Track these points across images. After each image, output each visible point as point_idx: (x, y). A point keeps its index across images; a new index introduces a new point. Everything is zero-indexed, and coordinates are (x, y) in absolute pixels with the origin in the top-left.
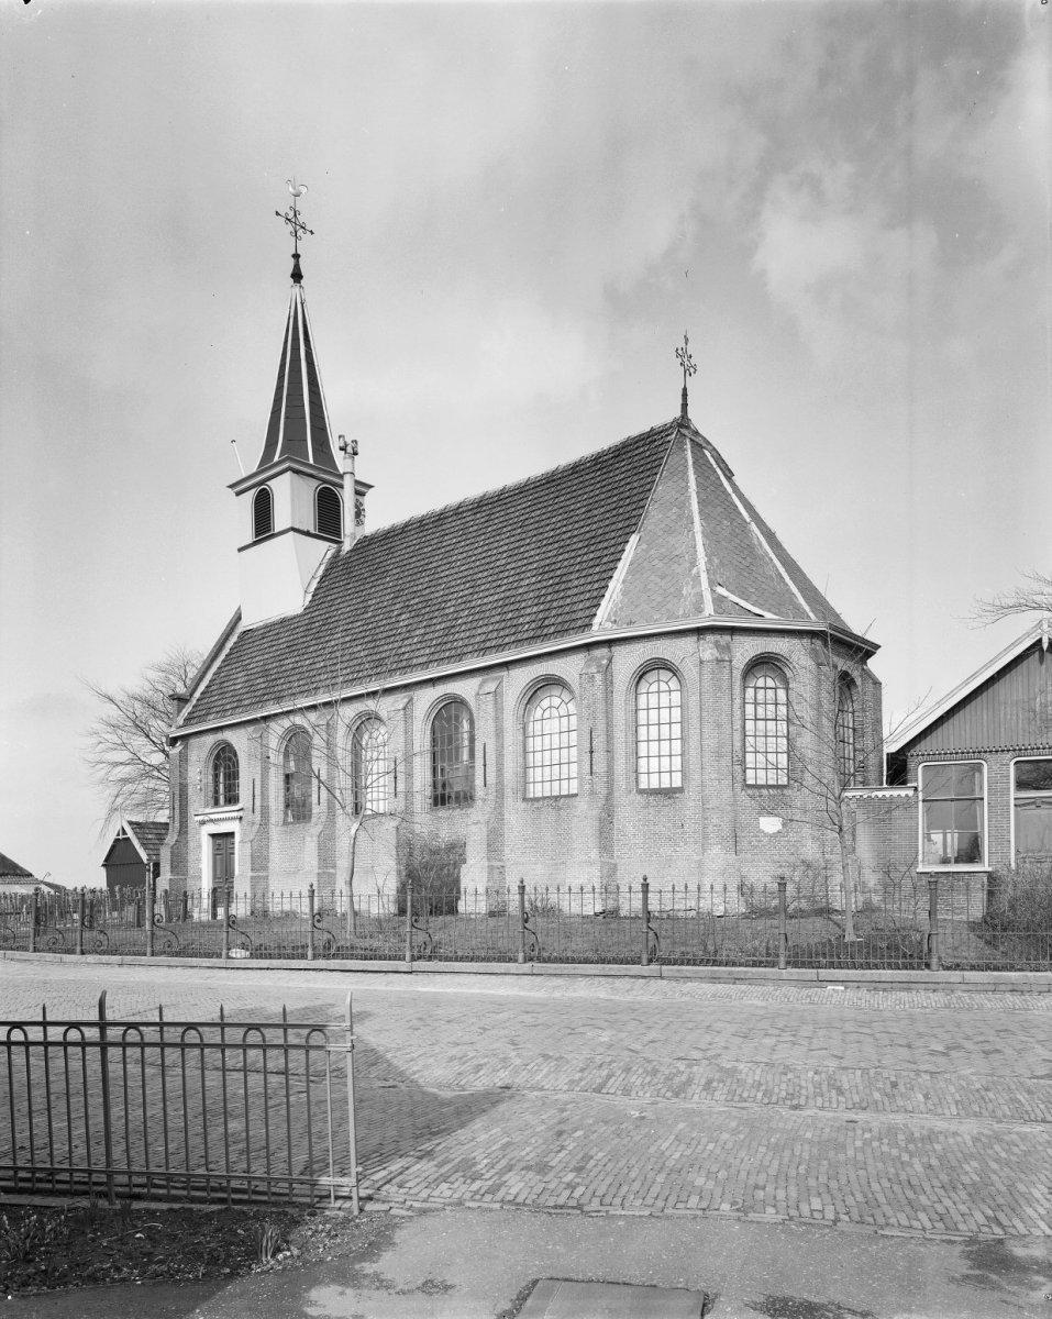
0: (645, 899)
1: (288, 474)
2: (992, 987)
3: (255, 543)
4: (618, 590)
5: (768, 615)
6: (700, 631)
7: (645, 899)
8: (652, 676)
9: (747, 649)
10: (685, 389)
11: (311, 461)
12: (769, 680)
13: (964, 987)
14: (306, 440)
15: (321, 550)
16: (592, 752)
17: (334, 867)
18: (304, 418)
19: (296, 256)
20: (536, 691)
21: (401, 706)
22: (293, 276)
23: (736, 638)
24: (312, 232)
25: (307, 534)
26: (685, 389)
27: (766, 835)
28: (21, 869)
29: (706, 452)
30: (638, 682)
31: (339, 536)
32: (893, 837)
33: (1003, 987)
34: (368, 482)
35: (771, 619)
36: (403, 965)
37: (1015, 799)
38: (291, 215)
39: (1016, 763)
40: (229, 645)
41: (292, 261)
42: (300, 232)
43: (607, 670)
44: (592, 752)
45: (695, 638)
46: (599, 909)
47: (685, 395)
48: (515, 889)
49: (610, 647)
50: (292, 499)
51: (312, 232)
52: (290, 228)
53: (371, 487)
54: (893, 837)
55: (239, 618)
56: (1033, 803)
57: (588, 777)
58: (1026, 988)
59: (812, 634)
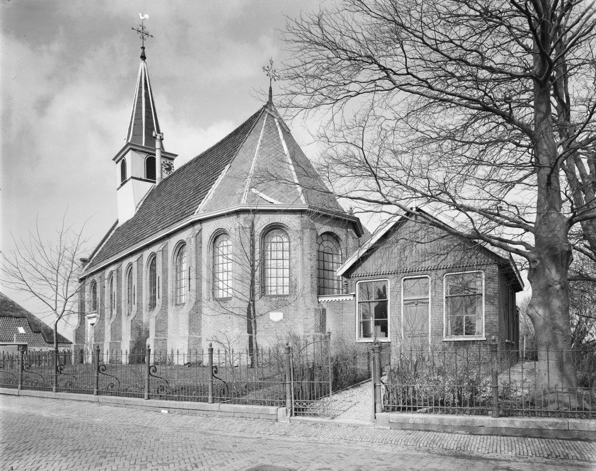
0: (211, 357)
1: (131, 151)
2: (232, 414)
3: (122, 185)
4: (212, 194)
5: (276, 202)
6: (237, 213)
7: (211, 357)
8: (219, 240)
9: (263, 221)
10: (271, 88)
11: (143, 145)
12: (278, 238)
13: (220, 414)
14: (142, 135)
15: (148, 186)
16: (190, 279)
17: (121, 339)
18: (142, 124)
19: (143, 48)
20: (180, 249)
21: (136, 260)
22: (141, 57)
23: (257, 216)
24: (152, 36)
25: (141, 179)
26: (271, 88)
27: (273, 322)
28: (67, 340)
29: (276, 120)
30: (214, 242)
31: (155, 179)
32: (344, 323)
33: (237, 415)
34: (175, 153)
35: (277, 204)
36: (15, 391)
37: (404, 300)
38: (140, 29)
39: (405, 280)
40: (111, 234)
41: (141, 50)
42: (145, 37)
43: (199, 234)
44: (190, 279)
45: (236, 217)
46: (186, 362)
47: (271, 91)
48: (206, 352)
49: (201, 223)
50: (136, 163)
51: (152, 36)
52: (140, 35)
53: (176, 156)
54: (344, 323)
55: (117, 222)
56: (413, 303)
57: (189, 293)
58: (248, 415)
59: (302, 212)
